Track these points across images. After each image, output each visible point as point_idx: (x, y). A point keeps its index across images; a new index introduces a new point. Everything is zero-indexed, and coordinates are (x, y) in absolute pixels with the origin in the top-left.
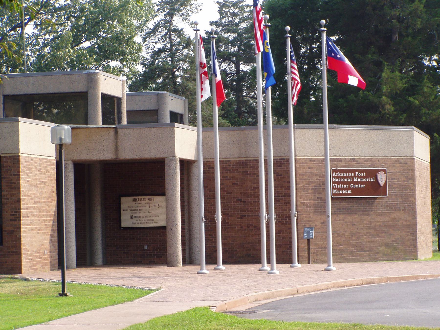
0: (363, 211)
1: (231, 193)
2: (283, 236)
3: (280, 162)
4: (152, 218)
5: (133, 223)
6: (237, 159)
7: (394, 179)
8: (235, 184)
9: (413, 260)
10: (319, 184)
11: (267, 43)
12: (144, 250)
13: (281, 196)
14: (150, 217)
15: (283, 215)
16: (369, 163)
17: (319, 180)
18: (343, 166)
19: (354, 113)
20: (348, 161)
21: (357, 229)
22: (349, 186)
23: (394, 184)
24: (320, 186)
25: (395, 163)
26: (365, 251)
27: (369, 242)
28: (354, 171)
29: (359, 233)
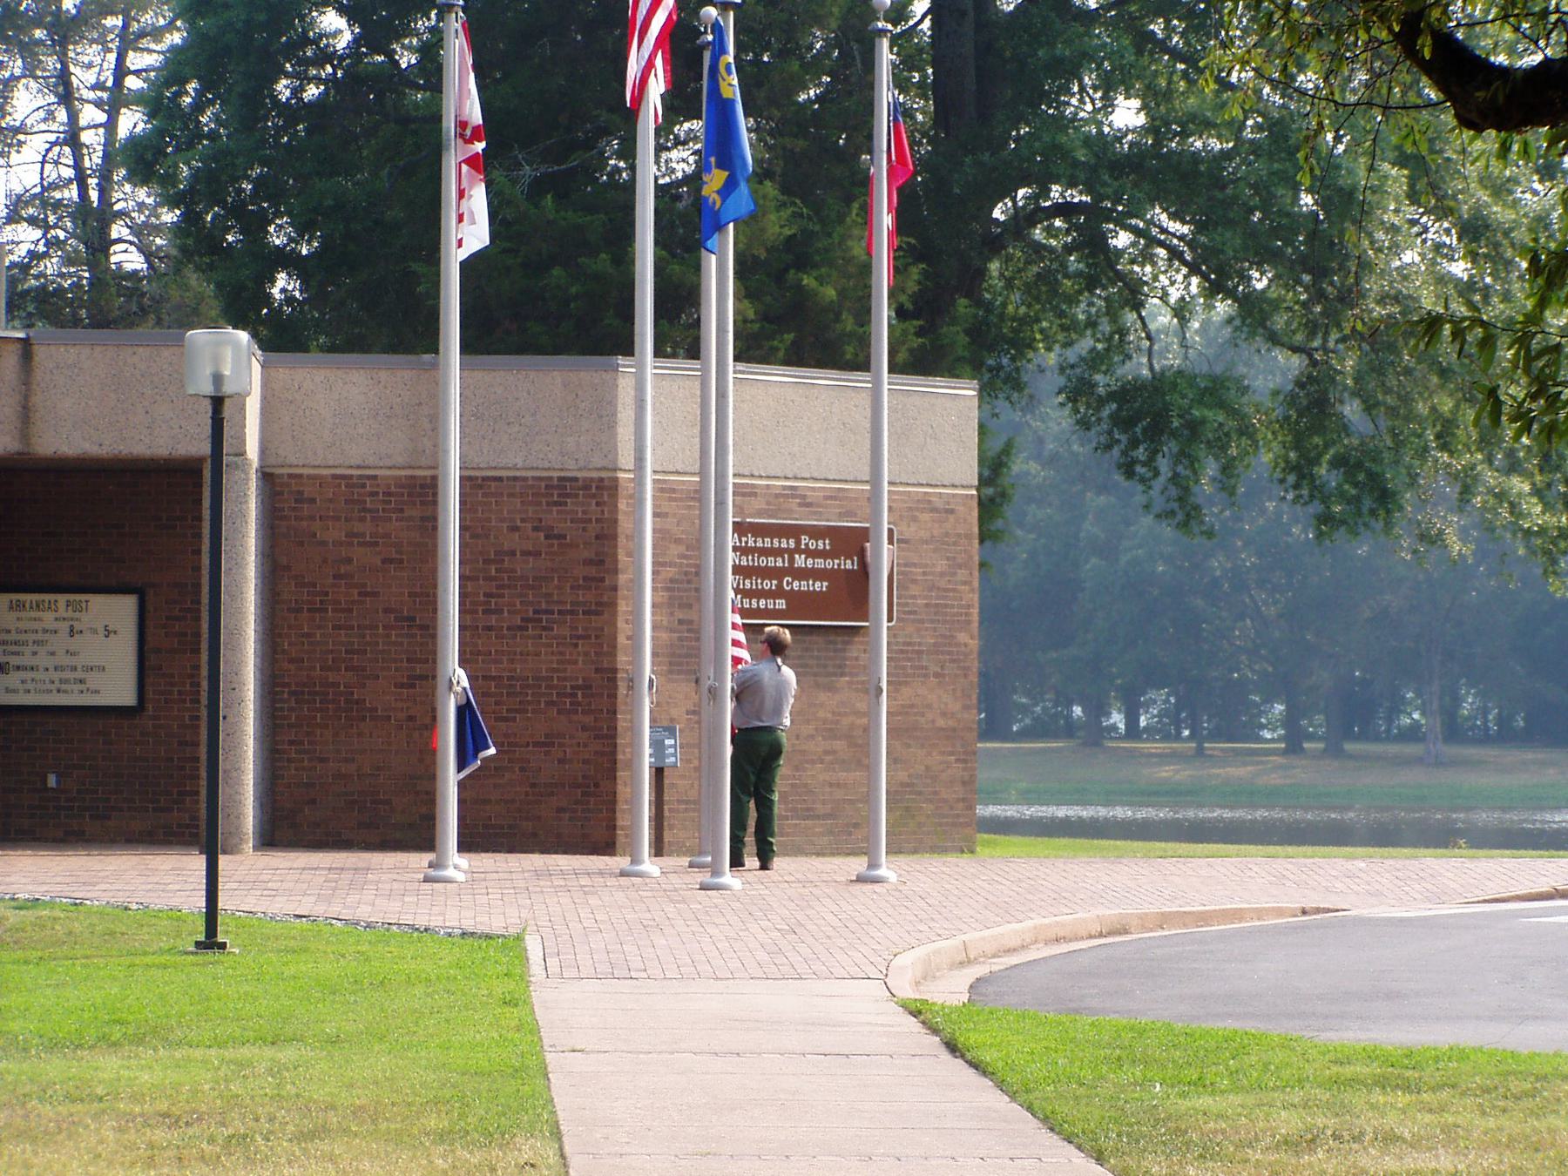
0: (815, 675)
1: (375, 594)
2: (561, 755)
3: (558, 487)
4: (79, 674)
5: (8, 690)
6: (403, 473)
7: (915, 565)
8: (391, 561)
9: (962, 852)
10: (686, 573)
11: (728, 66)
12: (46, 789)
13: (560, 612)
14: (74, 669)
15: (565, 679)
16: (841, 506)
17: (685, 557)
18: (759, 514)
19: (607, 321)
20: (777, 496)
21: (798, 737)
22: (780, 586)
23: (915, 581)
24: (689, 582)
25: (917, 509)
26: (818, 817)
27: (831, 785)
28: (794, 532)
29: (803, 752)
